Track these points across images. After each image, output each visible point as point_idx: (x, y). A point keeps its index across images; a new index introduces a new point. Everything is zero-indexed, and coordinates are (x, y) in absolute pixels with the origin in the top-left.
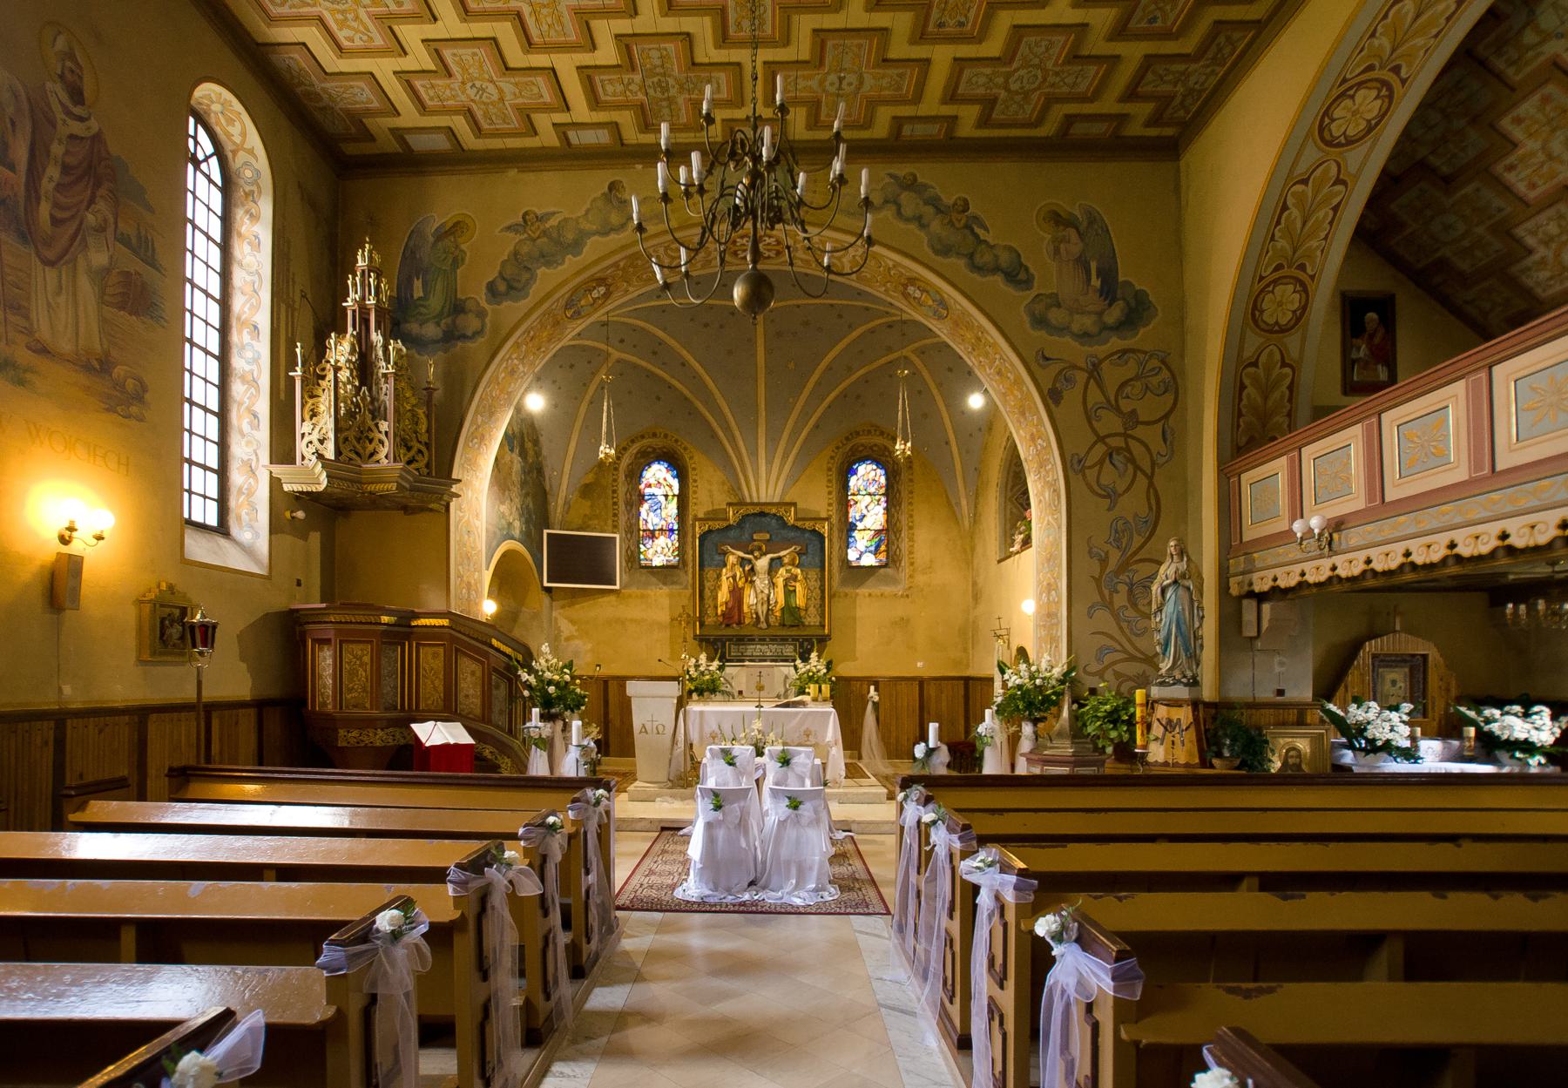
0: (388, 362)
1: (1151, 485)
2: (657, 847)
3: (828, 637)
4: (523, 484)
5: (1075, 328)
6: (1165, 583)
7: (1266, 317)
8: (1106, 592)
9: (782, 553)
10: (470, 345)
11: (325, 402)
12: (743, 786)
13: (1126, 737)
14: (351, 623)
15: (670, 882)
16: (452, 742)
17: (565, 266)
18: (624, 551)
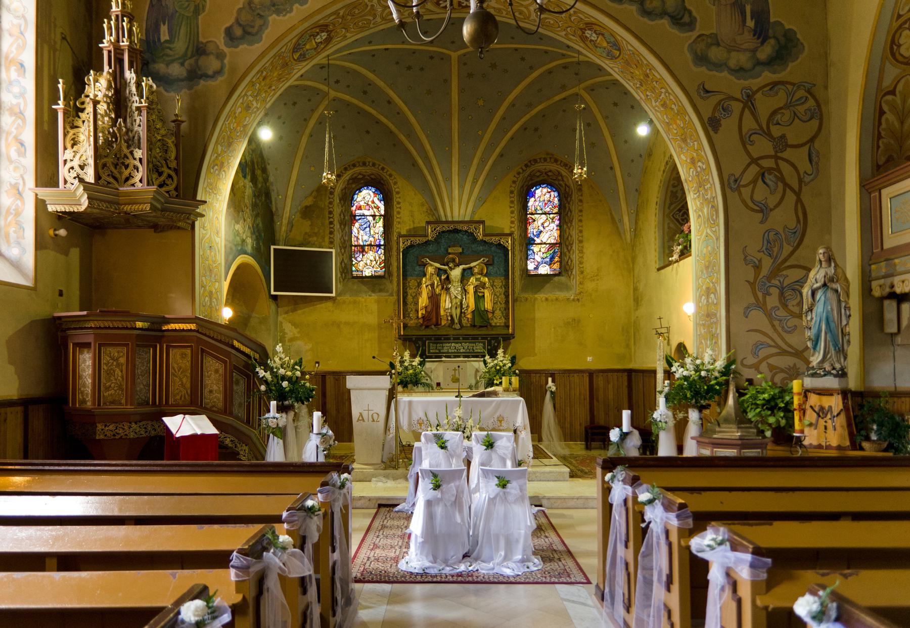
0: (141, 97)
1: (799, 200)
2: (377, 523)
3: (512, 336)
4: (254, 206)
5: (732, 63)
6: (816, 286)
7: (903, 50)
8: (760, 295)
9: (473, 264)
10: (211, 83)
11: (85, 133)
12: (454, 468)
13: (783, 422)
14: (109, 328)
15: (393, 555)
16: (199, 433)
17: (293, 14)
18: (339, 264)
